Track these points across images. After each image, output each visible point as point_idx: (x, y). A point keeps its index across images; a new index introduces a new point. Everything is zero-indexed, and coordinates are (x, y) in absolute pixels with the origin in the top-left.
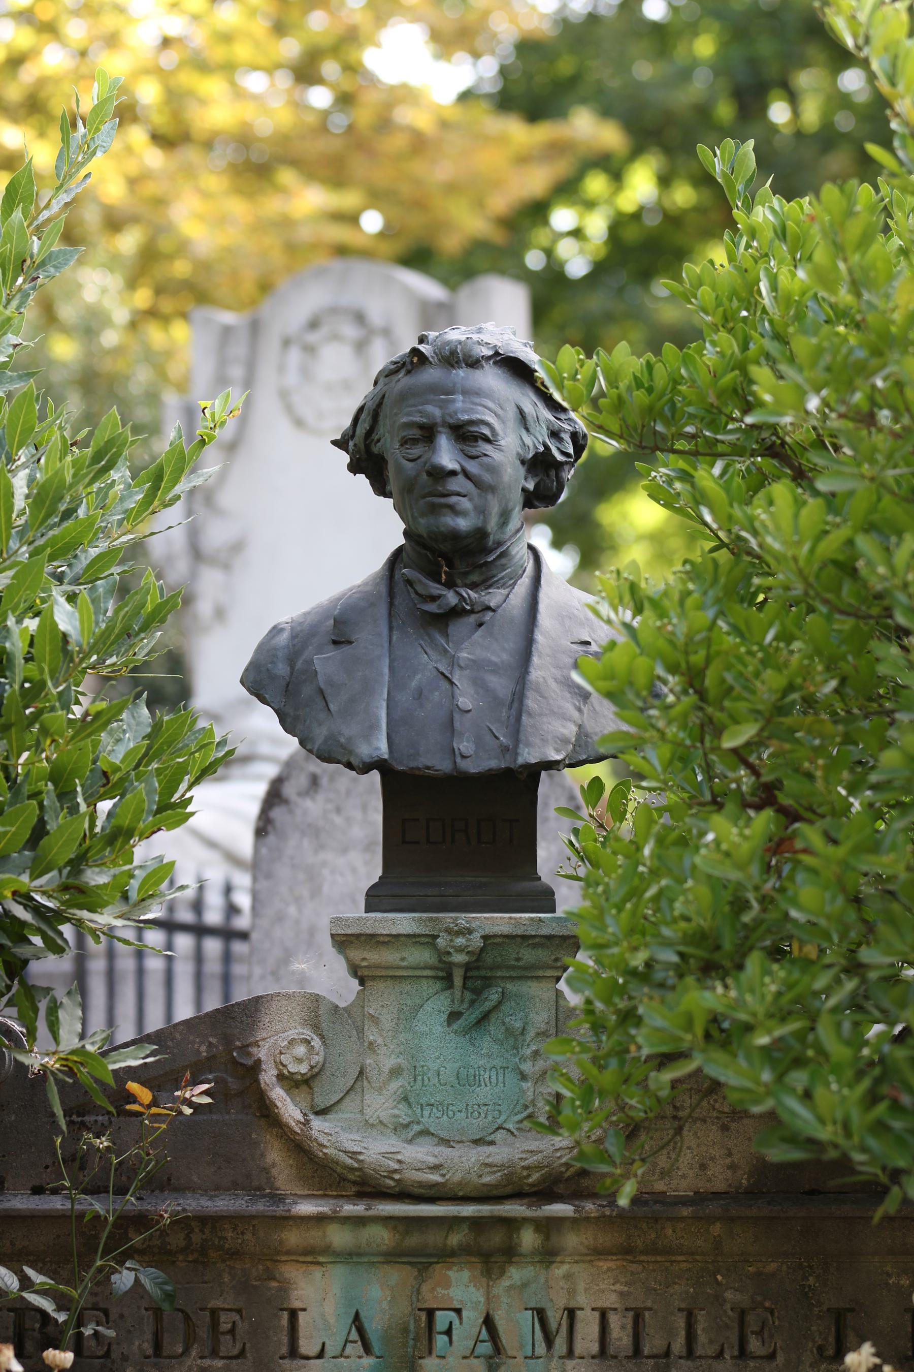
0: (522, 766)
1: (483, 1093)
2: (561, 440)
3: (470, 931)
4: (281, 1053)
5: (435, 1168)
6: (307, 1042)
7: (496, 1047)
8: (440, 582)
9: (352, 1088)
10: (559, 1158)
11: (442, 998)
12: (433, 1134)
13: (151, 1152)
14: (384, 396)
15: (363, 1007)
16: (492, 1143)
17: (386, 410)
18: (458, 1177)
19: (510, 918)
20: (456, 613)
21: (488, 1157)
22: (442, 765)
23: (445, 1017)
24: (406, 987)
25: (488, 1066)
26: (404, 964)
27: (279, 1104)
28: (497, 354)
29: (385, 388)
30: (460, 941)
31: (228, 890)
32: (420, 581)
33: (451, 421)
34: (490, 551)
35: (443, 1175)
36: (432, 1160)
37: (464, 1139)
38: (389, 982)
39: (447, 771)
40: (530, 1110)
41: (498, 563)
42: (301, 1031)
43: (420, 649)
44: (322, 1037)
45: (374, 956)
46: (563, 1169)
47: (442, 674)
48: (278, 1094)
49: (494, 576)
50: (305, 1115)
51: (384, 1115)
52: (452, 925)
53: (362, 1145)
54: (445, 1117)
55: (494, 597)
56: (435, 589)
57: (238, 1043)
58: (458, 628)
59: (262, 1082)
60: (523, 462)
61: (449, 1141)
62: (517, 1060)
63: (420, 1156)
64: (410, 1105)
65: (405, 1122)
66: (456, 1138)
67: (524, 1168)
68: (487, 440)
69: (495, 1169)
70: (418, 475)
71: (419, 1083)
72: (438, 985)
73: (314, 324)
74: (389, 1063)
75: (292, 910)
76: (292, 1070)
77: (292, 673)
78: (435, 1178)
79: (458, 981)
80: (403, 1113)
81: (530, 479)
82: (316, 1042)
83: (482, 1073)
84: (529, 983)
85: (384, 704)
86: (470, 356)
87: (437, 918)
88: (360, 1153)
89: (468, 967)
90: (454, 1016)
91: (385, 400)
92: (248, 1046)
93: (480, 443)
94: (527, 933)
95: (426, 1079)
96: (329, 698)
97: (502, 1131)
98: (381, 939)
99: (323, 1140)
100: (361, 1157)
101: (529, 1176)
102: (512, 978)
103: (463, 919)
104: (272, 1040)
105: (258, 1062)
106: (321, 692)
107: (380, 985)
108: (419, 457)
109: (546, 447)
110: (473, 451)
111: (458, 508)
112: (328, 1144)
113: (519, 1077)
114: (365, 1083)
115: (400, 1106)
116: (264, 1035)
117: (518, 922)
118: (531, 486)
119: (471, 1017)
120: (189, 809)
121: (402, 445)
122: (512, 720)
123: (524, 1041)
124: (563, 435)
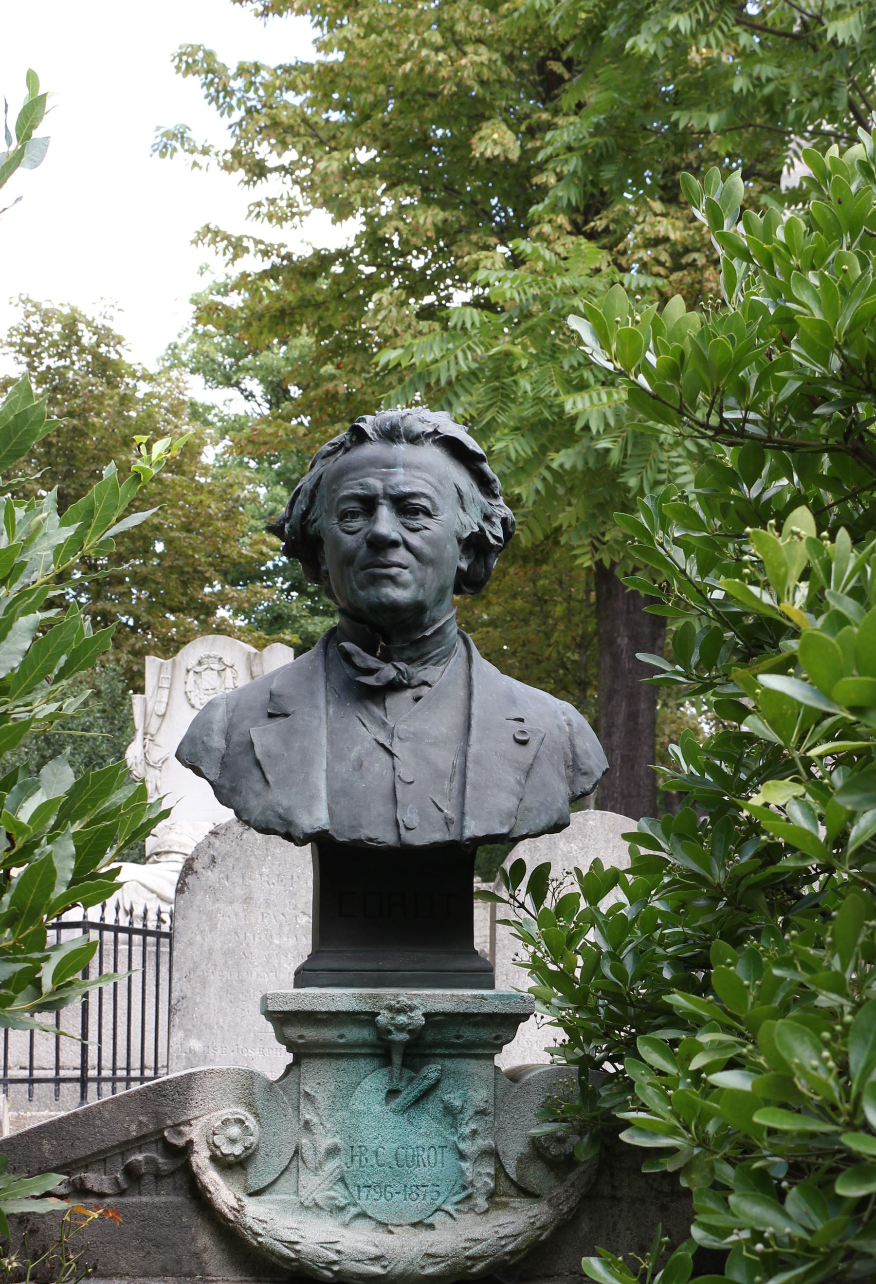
0: (469, 839)
1: (422, 1173)
2: (493, 524)
3: (412, 1008)
4: (214, 1134)
5: (377, 1259)
6: (240, 1122)
7: (435, 1125)
8: (375, 656)
9: (287, 1169)
10: (503, 1246)
11: (380, 1075)
12: (370, 1217)
13: (71, 1256)
14: (321, 477)
15: (299, 1084)
16: (431, 1226)
17: (323, 491)
18: (400, 1268)
19: (453, 995)
20: (395, 687)
21: (431, 1246)
22: (388, 837)
23: (384, 1095)
24: (343, 1064)
25: (427, 1146)
26: (342, 1041)
27: (212, 1189)
28: (436, 432)
29: (322, 469)
30: (402, 1019)
31: (159, 913)
32: (359, 654)
33: (393, 492)
34: (427, 628)
35: (385, 1267)
36: (374, 1251)
37: (402, 1222)
38: (326, 1061)
39: (390, 843)
40: (470, 1190)
41: (435, 639)
42: (235, 1110)
43: (358, 722)
44: (256, 1115)
45: (312, 1034)
46: (507, 1258)
47: (382, 745)
48: (211, 1177)
49: (429, 653)
50: (239, 1200)
51: (320, 1197)
52: (393, 1003)
53: (300, 1233)
54: (383, 1199)
55: (430, 673)
56: (372, 662)
57: (169, 1122)
58: (399, 702)
59: (194, 1165)
60: (460, 541)
61: (387, 1225)
62: (456, 1138)
63: (360, 1246)
64: (346, 1186)
65: (342, 1205)
66: (395, 1222)
67: (468, 1258)
68: (428, 514)
69: (439, 1260)
70: (359, 548)
71: (356, 1164)
72: (375, 1063)
73: (200, 663)
74: (326, 1142)
75: (199, 938)
76: (225, 1152)
77: (228, 746)
78: (377, 1269)
79: (397, 1060)
80: (340, 1195)
81: (464, 560)
82: (251, 1122)
83: (421, 1153)
84: (468, 1061)
85: (323, 775)
86: (411, 432)
87: (378, 995)
88: (297, 1243)
89: (407, 1045)
90: (392, 1093)
91: (323, 480)
92: (179, 1125)
93: (421, 516)
94: (469, 1011)
95: (363, 1159)
96: (266, 769)
97: (440, 1213)
98: (320, 1016)
99: (257, 1228)
100: (298, 1247)
101: (473, 1266)
102: (450, 1056)
103: (404, 995)
104: (204, 1120)
105: (190, 1142)
106: (258, 763)
107: (317, 1063)
108: (359, 530)
109: (481, 529)
110: (415, 524)
111: (400, 579)
112: (263, 1232)
113: (457, 1156)
114: (300, 1164)
115: (336, 1187)
116: (197, 1113)
117: (461, 1000)
118: (464, 565)
119: (408, 1095)
120: (119, 879)
121: (341, 520)
122: (455, 793)
123: (463, 1119)
124: (494, 519)
